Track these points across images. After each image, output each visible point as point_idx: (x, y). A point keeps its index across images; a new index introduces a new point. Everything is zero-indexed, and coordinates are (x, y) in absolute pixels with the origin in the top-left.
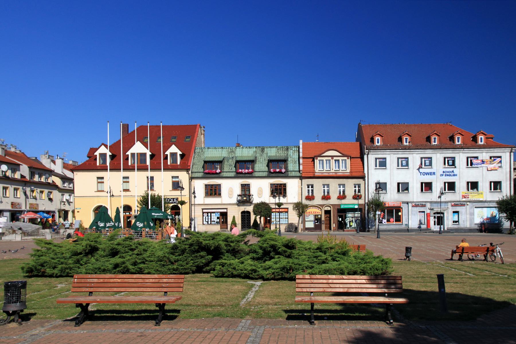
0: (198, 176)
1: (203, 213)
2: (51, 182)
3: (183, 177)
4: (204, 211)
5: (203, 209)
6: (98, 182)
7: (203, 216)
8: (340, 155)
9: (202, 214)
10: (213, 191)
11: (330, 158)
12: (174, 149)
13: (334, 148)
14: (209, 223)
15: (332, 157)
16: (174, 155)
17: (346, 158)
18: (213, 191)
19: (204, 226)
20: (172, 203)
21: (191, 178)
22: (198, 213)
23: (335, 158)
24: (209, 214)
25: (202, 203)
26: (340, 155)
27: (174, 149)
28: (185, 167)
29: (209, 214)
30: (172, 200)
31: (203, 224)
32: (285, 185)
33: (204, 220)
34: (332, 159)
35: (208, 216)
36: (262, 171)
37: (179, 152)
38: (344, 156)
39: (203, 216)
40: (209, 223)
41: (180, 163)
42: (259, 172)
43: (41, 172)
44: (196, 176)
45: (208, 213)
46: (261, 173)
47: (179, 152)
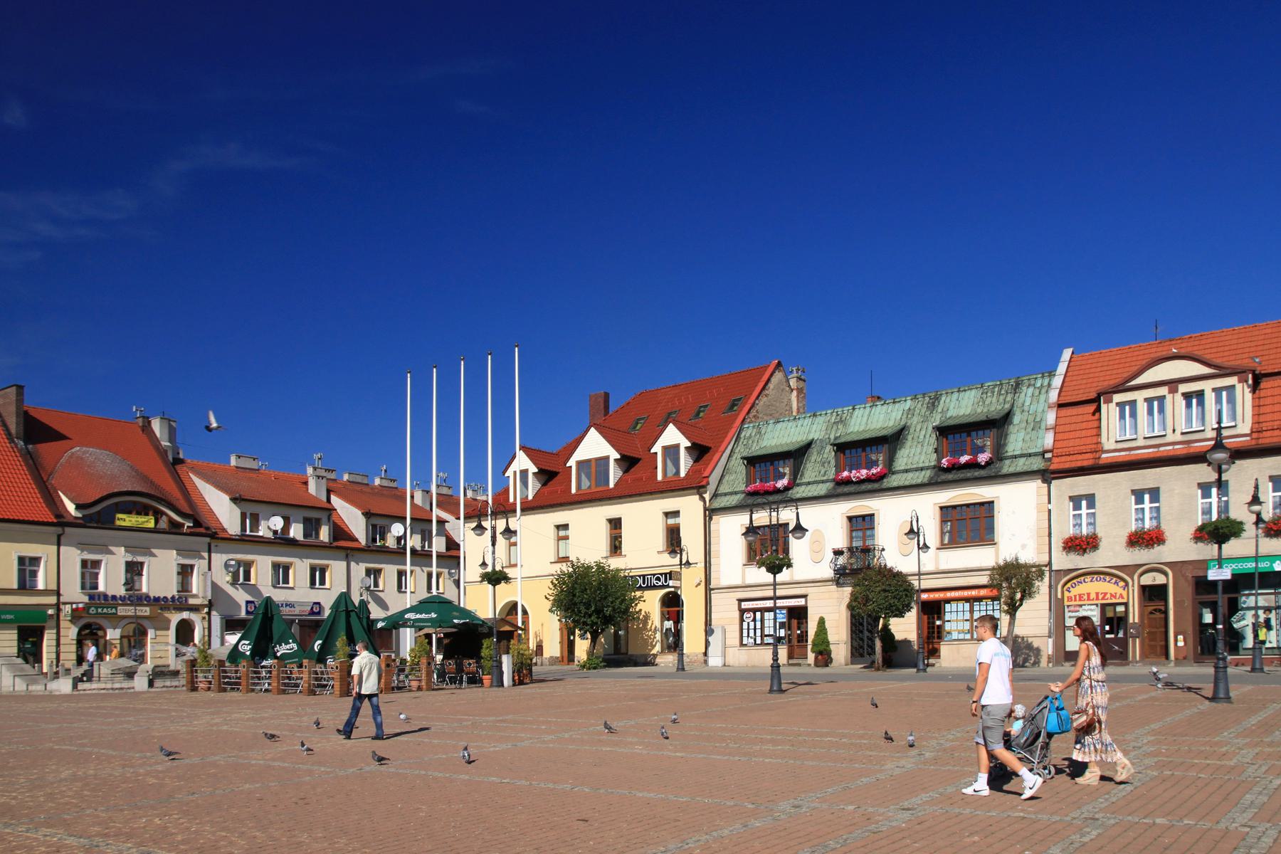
0: (728, 504)
1: (742, 612)
2: (270, 535)
3: (690, 508)
4: (745, 605)
5: (740, 601)
6: (560, 539)
7: (742, 620)
8: (1206, 370)
9: (737, 614)
10: (770, 548)
11: (1163, 391)
12: (672, 436)
13: (1198, 353)
14: (759, 641)
15: (1172, 384)
16: (671, 451)
17: (1232, 380)
18: (770, 548)
19: (744, 651)
20: (663, 587)
21: (710, 513)
22: (725, 610)
23: (1184, 388)
24: (758, 614)
25: (738, 582)
26: (1206, 370)
27: (672, 436)
28: (694, 485)
29: (758, 614)
30: (663, 579)
31: (742, 644)
32: (987, 507)
33: (745, 633)
34: (1173, 391)
35: (754, 620)
36: (917, 470)
37: (685, 443)
38: (1223, 372)
39: (742, 620)
40: (759, 641)
41: (616, 485)
42: (907, 471)
43: (288, 512)
44: (722, 505)
45: (754, 611)
46: (910, 475)
47: (685, 443)
